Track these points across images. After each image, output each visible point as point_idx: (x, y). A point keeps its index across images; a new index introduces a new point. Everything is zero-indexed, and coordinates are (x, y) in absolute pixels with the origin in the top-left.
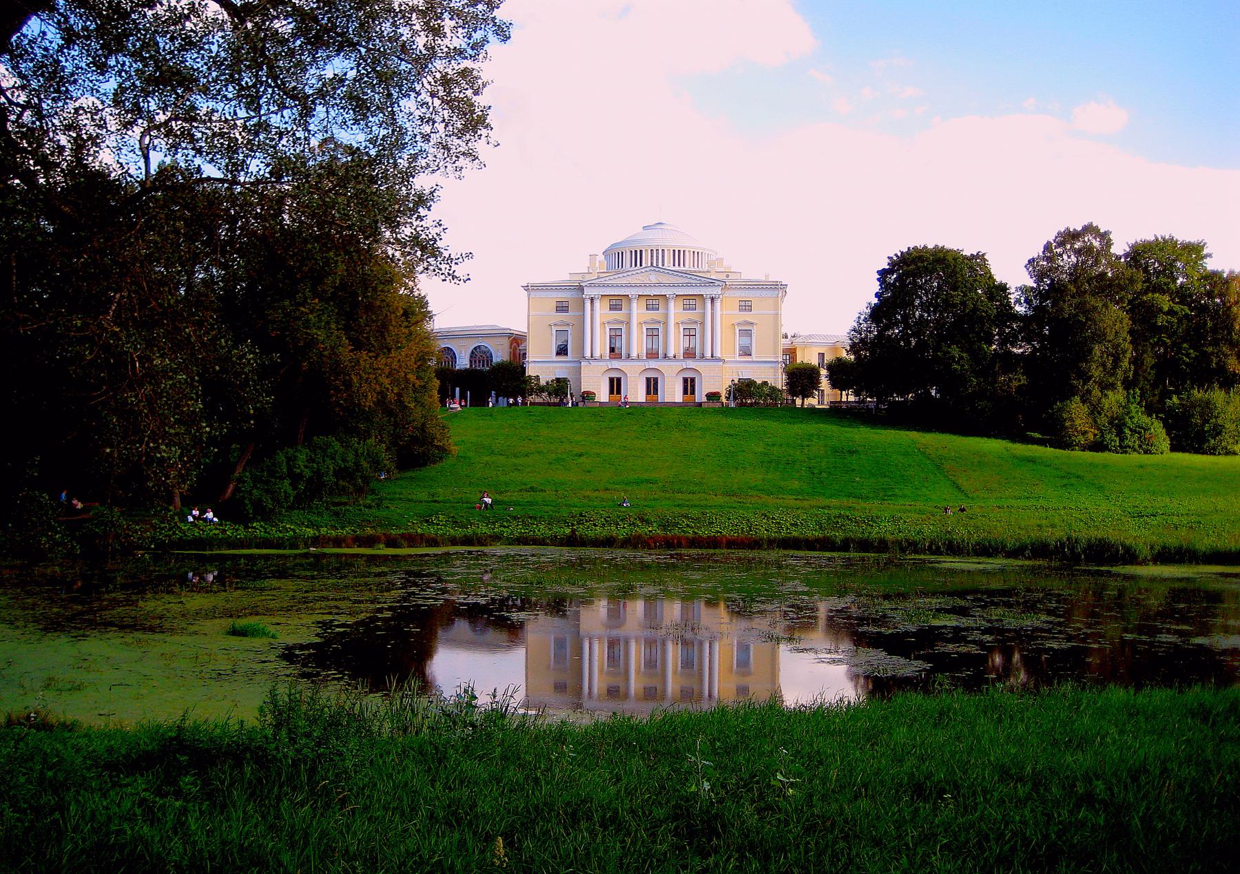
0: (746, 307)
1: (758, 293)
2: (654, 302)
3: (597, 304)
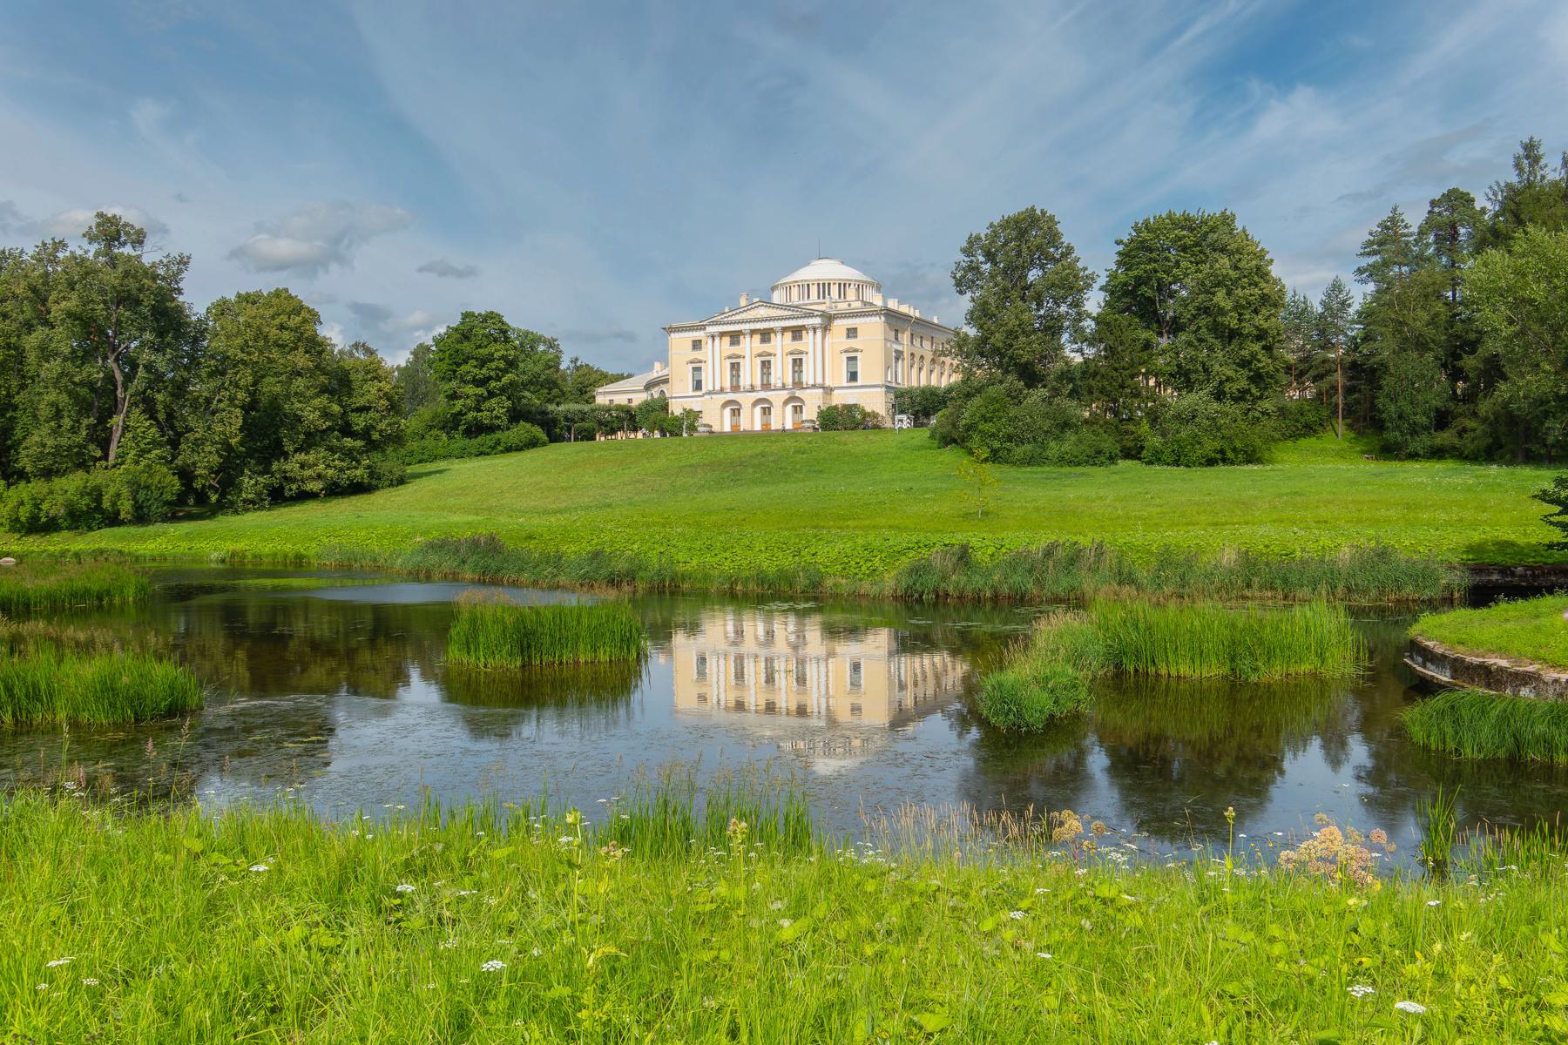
0: (852, 333)
1: (863, 320)
2: (766, 335)
3: (717, 340)
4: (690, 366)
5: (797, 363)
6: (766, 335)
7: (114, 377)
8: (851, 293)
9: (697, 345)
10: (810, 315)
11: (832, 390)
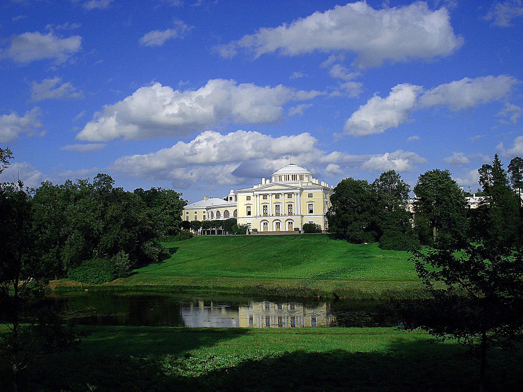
0: (310, 196)
3: (258, 197)
4: (246, 206)
5: (290, 206)
6: (277, 196)
7: (130, 296)
8: (306, 179)
9: (248, 198)
10: (296, 188)
11: (303, 216)
